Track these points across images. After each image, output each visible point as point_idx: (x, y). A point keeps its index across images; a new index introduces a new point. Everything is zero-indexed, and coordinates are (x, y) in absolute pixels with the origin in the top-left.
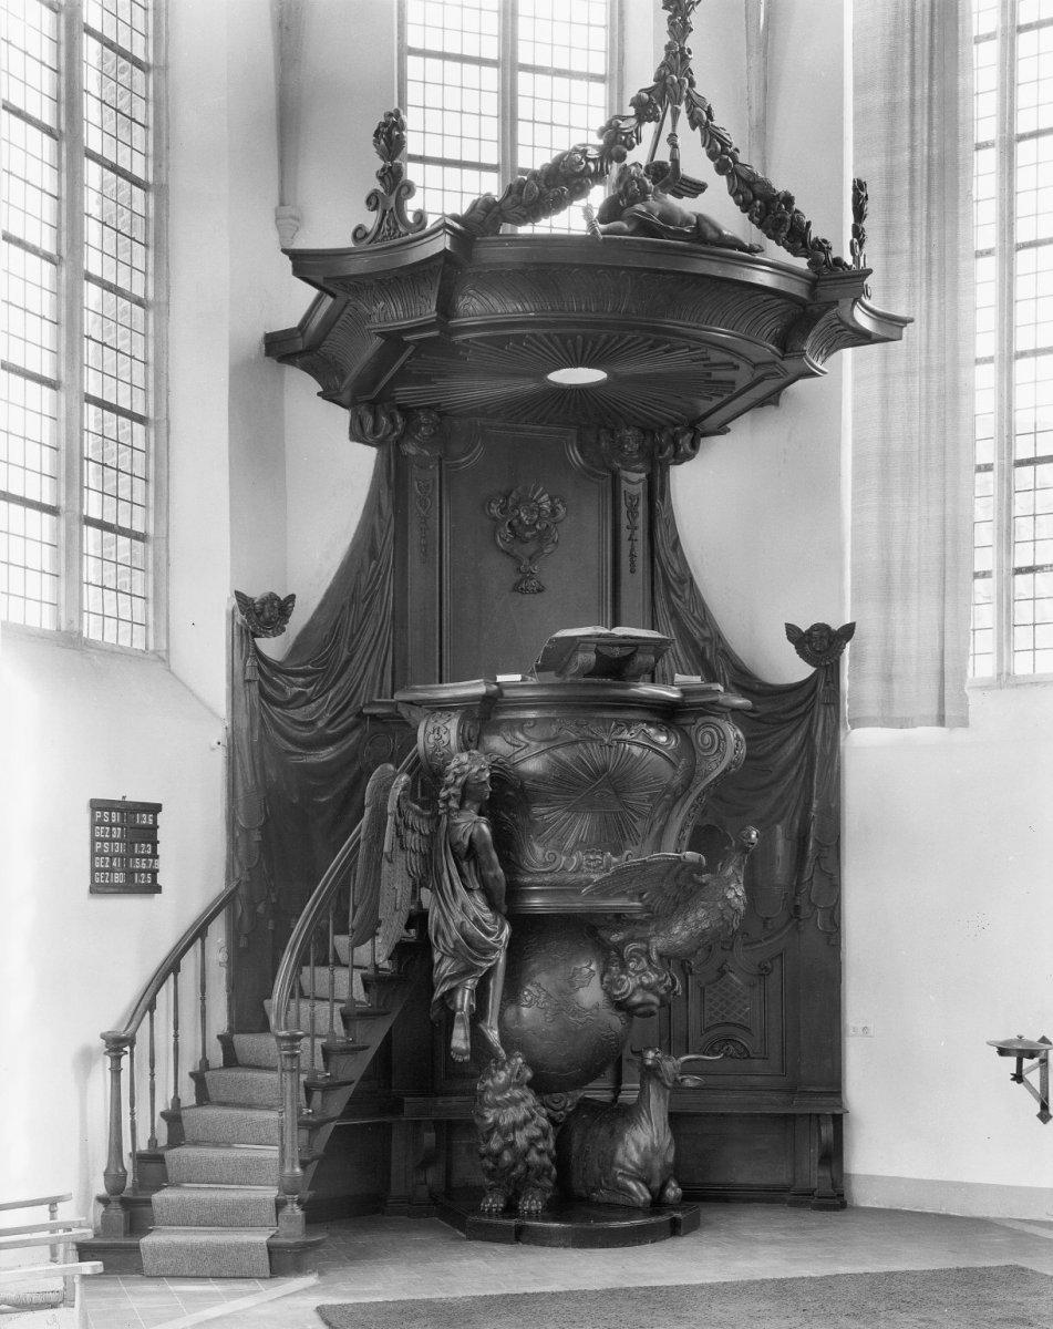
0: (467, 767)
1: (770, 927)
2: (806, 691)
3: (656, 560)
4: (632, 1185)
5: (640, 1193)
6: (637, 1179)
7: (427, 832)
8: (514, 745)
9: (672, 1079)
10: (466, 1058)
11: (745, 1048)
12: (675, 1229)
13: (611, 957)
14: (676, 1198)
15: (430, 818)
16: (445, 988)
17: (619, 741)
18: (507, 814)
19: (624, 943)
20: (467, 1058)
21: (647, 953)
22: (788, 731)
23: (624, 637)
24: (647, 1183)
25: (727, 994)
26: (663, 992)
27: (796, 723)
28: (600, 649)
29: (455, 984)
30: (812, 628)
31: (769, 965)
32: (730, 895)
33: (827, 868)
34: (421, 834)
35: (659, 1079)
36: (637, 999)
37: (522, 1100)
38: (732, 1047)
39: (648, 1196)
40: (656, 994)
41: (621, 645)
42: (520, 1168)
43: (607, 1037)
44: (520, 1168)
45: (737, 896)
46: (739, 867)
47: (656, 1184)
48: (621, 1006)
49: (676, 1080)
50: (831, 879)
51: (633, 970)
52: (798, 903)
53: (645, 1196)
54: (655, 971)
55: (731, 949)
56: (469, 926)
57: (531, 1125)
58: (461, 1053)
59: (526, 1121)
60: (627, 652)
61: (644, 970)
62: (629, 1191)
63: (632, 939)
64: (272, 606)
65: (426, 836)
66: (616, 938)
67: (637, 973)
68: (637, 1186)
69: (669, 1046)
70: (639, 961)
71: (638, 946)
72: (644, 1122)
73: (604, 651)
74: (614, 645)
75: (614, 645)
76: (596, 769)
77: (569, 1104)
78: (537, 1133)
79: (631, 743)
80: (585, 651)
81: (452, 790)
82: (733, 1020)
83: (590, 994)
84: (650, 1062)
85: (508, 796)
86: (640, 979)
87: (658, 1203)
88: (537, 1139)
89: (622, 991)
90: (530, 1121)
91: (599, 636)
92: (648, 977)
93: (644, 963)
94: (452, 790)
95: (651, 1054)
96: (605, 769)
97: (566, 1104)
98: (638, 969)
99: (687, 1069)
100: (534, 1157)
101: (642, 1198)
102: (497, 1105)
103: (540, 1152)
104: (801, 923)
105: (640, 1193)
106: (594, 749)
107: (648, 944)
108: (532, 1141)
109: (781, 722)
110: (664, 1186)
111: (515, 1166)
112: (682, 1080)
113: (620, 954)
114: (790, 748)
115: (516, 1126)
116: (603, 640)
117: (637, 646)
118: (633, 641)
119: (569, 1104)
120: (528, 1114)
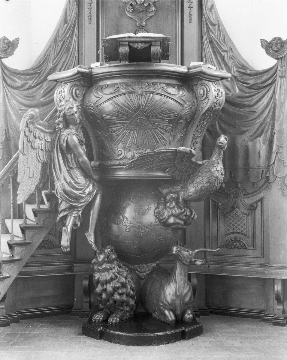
0: (63, 107)
1: (256, 187)
2: (273, 70)
3: (203, 17)
4: (167, 312)
5: (170, 316)
6: (170, 310)
7: (50, 140)
8: (97, 97)
9: (188, 260)
10: (68, 250)
11: (244, 244)
12: (183, 336)
13: (161, 200)
14: (190, 319)
15: (51, 133)
16: (61, 215)
17: (147, 92)
18: (100, 131)
19: (167, 194)
20: (68, 250)
21: (178, 198)
22: (264, 92)
23: (143, 37)
24: (174, 312)
25: (235, 219)
26: (184, 218)
27: (268, 88)
28: (131, 44)
29: (66, 213)
30: (273, 40)
31: (255, 205)
32: (214, 170)
33: (281, 157)
34: (46, 141)
35: (180, 261)
36: (171, 220)
37: (111, 269)
38: (238, 244)
39: (173, 318)
40: (181, 219)
41: (142, 42)
42: (111, 301)
43: (158, 239)
44: (111, 301)
45: (217, 170)
46: (219, 156)
47: (179, 312)
48: (165, 224)
49: (191, 261)
50: (284, 163)
51: (169, 207)
52: (268, 175)
53: (171, 317)
54: (179, 207)
55: (238, 197)
56: (68, 188)
57: (115, 281)
58: (66, 248)
59: (112, 279)
60: (146, 46)
61: (174, 207)
62: (165, 315)
63: (172, 193)
64: (4, 42)
65: (49, 142)
66: (165, 191)
67: (171, 208)
68: (170, 313)
69: (184, 243)
70: (171, 203)
71: (173, 195)
72: (174, 281)
73: (135, 46)
74: (138, 42)
75: (138, 42)
76: (136, 108)
77: (147, 270)
78: (119, 285)
79: (154, 93)
80: (123, 46)
81: (60, 119)
82: (239, 231)
83: (150, 218)
84: (174, 253)
85: (98, 123)
86: (172, 211)
87: (180, 321)
88: (118, 288)
89: (163, 217)
90: (114, 279)
91: (130, 37)
92: (175, 211)
93: (174, 204)
94: (60, 119)
95: (175, 248)
96: (139, 107)
97: (146, 269)
98: (171, 206)
99: (197, 256)
100: (117, 296)
101: (170, 319)
102: (99, 271)
103: (120, 294)
104: (269, 185)
105: (170, 316)
106: (133, 97)
107: (178, 195)
108: (115, 289)
109: (260, 88)
110: (184, 313)
111: (108, 300)
112: (195, 261)
113: (165, 198)
114: (265, 100)
115: (107, 282)
116: (131, 40)
117: (150, 42)
118: (148, 39)
119: (147, 270)
120: (114, 276)
